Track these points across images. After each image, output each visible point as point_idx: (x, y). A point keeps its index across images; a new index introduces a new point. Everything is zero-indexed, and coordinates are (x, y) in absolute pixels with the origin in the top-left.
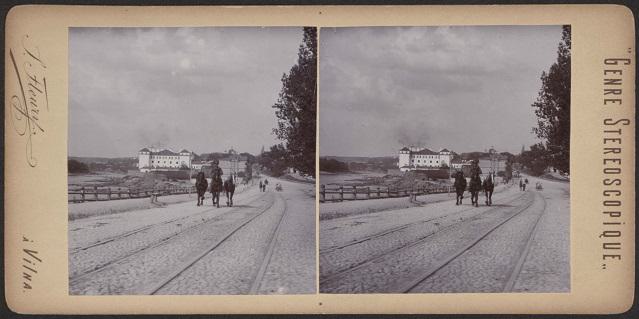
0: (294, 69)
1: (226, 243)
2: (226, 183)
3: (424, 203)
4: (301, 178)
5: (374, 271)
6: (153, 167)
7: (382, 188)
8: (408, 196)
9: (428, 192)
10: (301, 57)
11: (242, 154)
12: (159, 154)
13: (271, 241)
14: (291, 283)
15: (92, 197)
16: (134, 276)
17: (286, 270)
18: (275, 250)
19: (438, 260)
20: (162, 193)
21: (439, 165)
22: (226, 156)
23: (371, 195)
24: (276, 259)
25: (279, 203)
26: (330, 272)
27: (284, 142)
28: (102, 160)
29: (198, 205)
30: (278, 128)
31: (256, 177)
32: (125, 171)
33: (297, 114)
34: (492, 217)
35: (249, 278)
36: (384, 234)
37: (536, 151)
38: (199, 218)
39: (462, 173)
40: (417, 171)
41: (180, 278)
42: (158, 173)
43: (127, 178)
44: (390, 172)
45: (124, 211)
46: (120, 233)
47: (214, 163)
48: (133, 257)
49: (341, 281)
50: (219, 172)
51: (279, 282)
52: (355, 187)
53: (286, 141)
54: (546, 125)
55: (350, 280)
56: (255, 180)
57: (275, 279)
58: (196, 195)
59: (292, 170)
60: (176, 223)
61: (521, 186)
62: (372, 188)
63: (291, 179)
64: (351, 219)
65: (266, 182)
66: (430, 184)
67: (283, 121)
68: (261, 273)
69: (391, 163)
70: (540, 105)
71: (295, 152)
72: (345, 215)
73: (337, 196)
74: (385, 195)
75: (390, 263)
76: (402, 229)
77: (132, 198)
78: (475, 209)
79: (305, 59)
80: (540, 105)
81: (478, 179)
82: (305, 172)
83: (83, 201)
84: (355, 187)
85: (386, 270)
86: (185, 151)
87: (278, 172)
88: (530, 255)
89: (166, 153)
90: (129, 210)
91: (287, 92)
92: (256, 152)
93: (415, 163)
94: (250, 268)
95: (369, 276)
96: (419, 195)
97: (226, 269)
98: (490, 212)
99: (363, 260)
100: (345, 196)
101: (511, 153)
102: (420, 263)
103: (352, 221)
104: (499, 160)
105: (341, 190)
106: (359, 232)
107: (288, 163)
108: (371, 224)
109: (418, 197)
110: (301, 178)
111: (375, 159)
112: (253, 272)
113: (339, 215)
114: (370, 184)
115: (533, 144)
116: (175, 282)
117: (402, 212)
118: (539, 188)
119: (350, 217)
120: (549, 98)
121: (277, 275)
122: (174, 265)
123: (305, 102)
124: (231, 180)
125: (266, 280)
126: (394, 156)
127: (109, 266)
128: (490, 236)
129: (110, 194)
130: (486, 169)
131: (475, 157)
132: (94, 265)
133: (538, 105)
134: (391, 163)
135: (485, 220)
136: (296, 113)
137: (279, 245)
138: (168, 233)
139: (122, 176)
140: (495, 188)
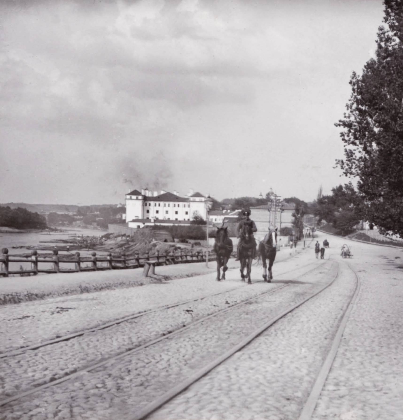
0: (370, 66)
1: (261, 339)
2: (262, 245)
3: (167, 278)
4: (381, 237)
5: (89, 386)
6: (148, 220)
7: (100, 254)
8: (142, 266)
9: (174, 261)
10: (380, 47)
11: (288, 201)
12: (159, 199)
13: (334, 334)
14: (365, 403)
15: (50, 266)
16: (114, 390)
17: (358, 383)
18: (341, 351)
19: (192, 367)
20: (161, 260)
21: (190, 217)
22: (261, 203)
23: (83, 265)
24: (342, 365)
25: (346, 281)
26: (17, 387)
27: (355, 181)
28: (67, 208)
29: (219, 279)
30: (344, 158)
31: (309, 236)
32: (104, 226)
33: (373, 137)
34: (278, 300)
35: (299, 394)
36: (105, 327)
37: (341, 195)
38: (220, 301)
39: (225, 230)
40: (155, 228)
41: (189, 394)
42: (157, 228)
43: (107, 236)
44: (113, 229)
45: (101, 289)
46: (93, 324)
47: (243, 213)
48: (112, 361)
49: (36, 402)
50: (250, 227)
51: (346, 401)
52: (56, 253)
53: (358, 178)
54: (358, 155)
55: (50, 399)
56: (308, 241)
57: (342, 397)
58: (214, 264)
59: (366, 225)
60: (186, 307)
61: (317, 250)
62: (84, 253)
63: (365, 239)
64: (51, 303)
65: (326, 244)
66: (176, 249)
67: (351, 147)
68: (320, 381)
69: (113, 214)
70: (350, 125)
71: (372, 196)
72: (41, 297)
73: (28, 267)
74: (105, 265)
75: (115, 372)
76: (133, 319)
77: (114, 268)
78: (245, 284)
79: (386, 50)
80: (350, 125)
81: (252, 240)
82: (389, 229)
83: (35, 273)
84: (56, 253)
85: (110, 383)
86: (198, 195)
87: (344, 229)
88: (338, 361)
89: (168, 197)
90: (108, 287)
91: (358, 102)
92: (310, 197)
93: (152, 215)
94: (301, 379)
95: (81, 394)
96: (159, 264)
97: (261, 380)
98: (272, 292)
99: (71, 368)
100: (41, 266)
101: (301, 199)
102: (164, 373)
103: (54, 306)
104: (283, 210)
105: (35, 257)
106: (65, 323)
107: (360, 215)
108: (82, 311)
109: (158, 269)
110: (381, 237)
111: (88, 208)
112: (305, 385)
113: (31, 297)
114: (80, 248)
115: (336, 185)
116: (181, 399)
117: (134, 291)
118: (346, 254)
119: (50, 300)
120: (362, 113)
121: (343, 390)
122: (179, 374)
123: (387, 118)
124: (270, 241)
125: (325, 399)
126: (117, 202)
127: (73, 376)
128: (272, 329)
129: (79, 261)
130: (264, 223)
131: (245, 205)
132: (49, 374)
133: (345, 124)
134: (113, 214)
135: (265, 304)
136: (373, 137)
137: (347, 343)
138: (168, 324)
139: (99, 233)
140: (278, 254)
